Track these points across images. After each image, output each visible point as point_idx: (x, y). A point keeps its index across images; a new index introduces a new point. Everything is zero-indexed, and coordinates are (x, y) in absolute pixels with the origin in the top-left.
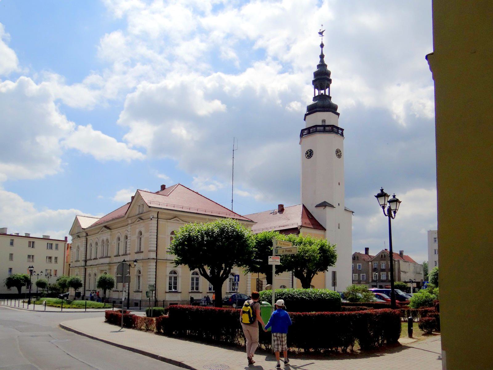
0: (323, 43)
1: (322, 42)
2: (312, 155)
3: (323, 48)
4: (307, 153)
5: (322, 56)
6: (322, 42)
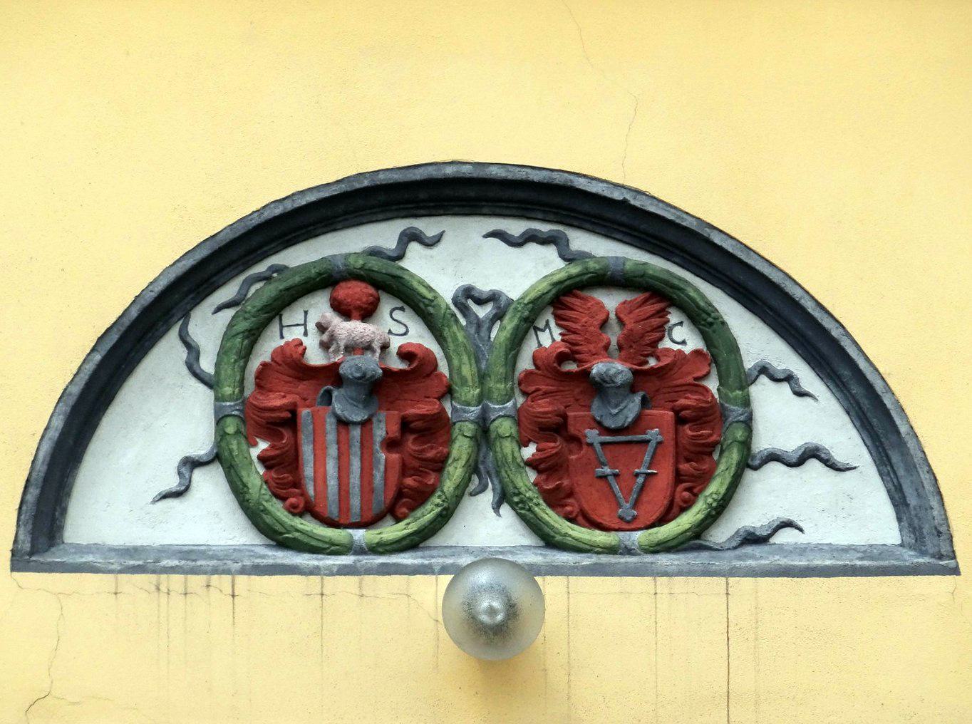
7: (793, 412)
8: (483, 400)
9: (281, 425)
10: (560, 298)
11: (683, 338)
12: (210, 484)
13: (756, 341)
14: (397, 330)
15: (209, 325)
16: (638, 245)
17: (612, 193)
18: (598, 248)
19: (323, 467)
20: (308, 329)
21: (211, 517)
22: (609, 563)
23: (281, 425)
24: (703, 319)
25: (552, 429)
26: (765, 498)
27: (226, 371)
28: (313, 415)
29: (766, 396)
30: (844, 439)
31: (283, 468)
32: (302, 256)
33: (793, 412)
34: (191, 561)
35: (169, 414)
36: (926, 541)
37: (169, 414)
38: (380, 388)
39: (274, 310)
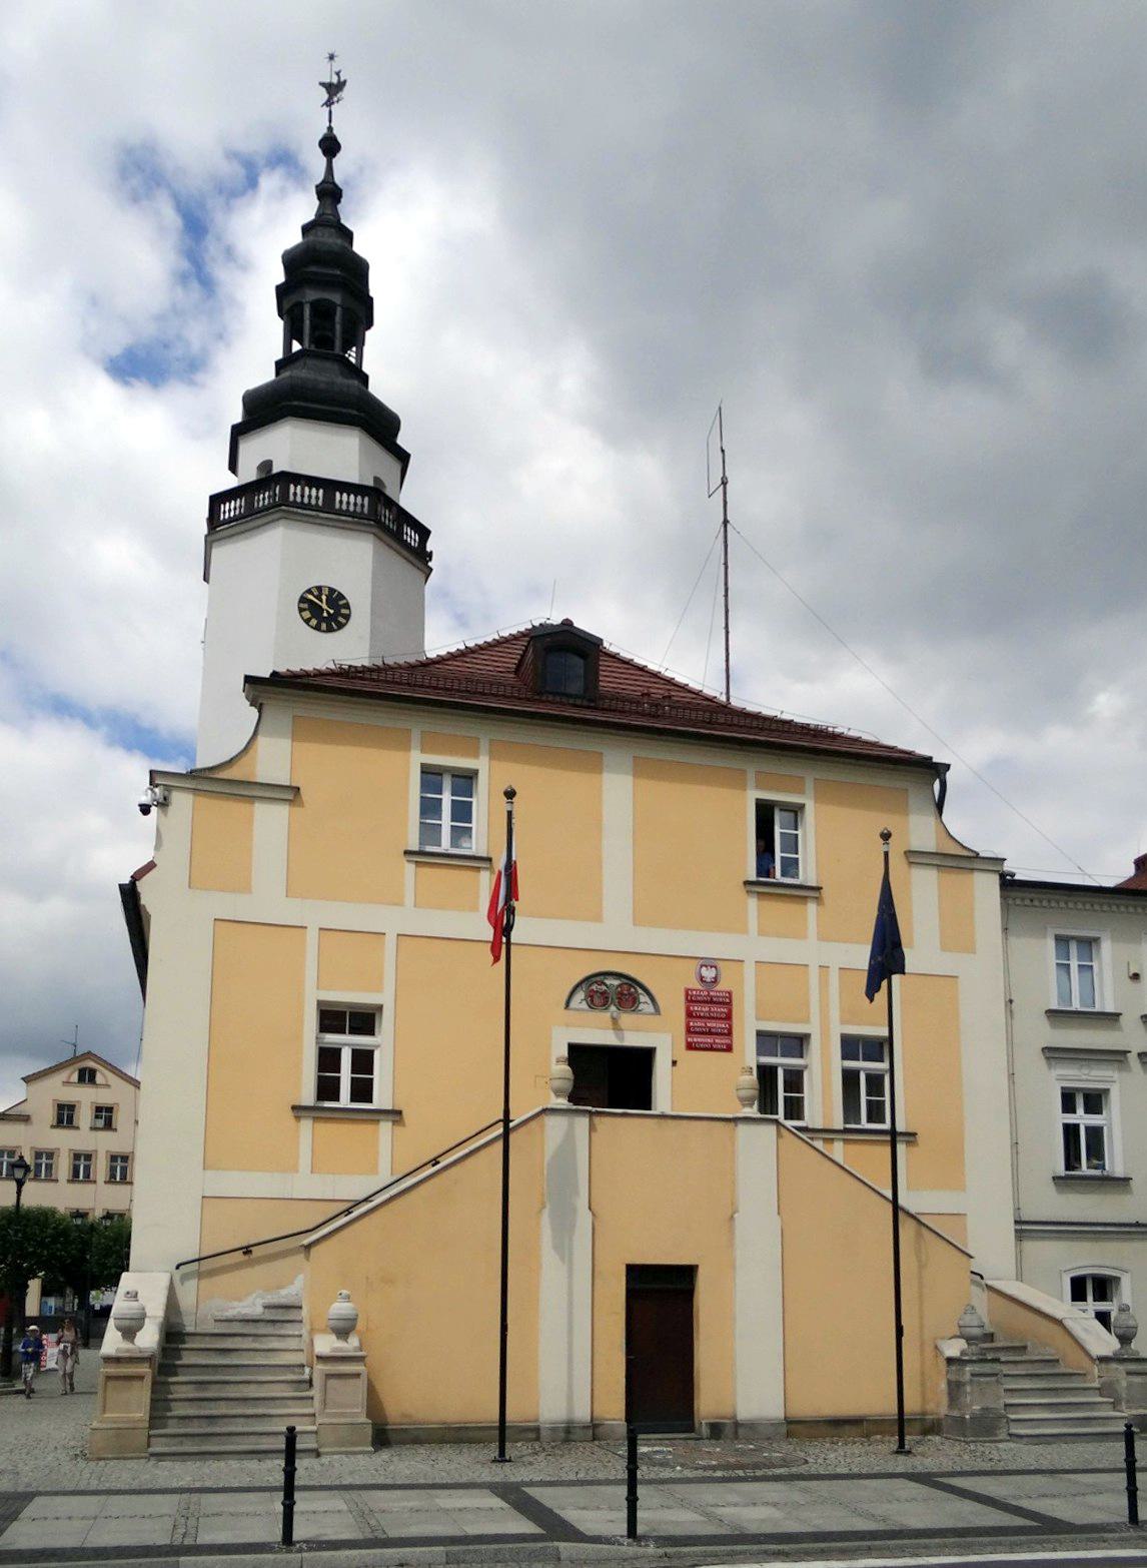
0: (335, 132)
1: (330, 129)
2: (307, 615)
3: (334, 161)
4: (336, 599)
5: (329, 193)
6: (330, 129)
7: (644, 998)
8: (613, 995)
9: (592, 997)
10: (620, 986)
11: (632, 990)
12: (584, 1002)
13: (640, 991)
14: (604, 988)
15: (584, 985)
16: (454, 665)
17: (1141, 1470)
18: (626, 981)
19: (597, 1000)
20: (594, 987)
21: (584, 1005)
22: (625, 1012)
23: (592, 997)
24: (635, 989)
25: (619, 998)
26: (641, 1007)
27: (58, 1250)
28: (141, 1378)
29: (641, 996)
30: (649, 1001)
31: (592, 1001)
32: (594, 979)
33: (644, 998)
34: (583, 1010)
35: (580, 995)
36: (657, 1011)
37: (580, 995)
38: (601, 993)
39: (591, 985)
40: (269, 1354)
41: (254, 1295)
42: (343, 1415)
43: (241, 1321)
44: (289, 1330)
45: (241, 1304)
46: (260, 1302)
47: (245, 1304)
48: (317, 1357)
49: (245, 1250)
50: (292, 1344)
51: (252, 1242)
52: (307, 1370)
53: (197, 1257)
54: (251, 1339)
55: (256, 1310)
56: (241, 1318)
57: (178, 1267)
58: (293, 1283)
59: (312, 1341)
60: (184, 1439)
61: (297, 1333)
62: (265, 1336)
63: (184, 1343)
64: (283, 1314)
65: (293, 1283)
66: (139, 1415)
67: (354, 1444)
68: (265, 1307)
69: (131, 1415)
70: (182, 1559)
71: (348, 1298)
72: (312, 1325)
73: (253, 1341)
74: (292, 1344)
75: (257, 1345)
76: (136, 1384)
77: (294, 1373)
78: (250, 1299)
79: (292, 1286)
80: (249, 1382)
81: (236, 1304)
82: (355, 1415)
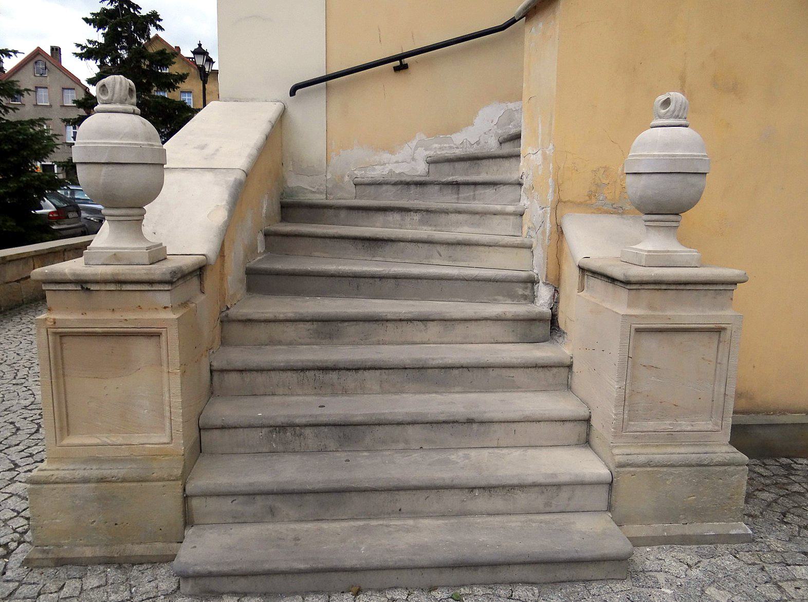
40: (459, 252)
41: (414, 143)
42: (672, 437)
43: (395, 184)
44: (487, 200)
45: (394, 158)
46: (422, 154)
47: (399, 157)
48: (582, 270)
49: (397, 63)
50: (499, 230)
51: (407, 49)
52: (544, 294)
53: (323, 74)
54: (417, 217)
55: (419, 169)
56: (395, 179)
57: (293, 92)
58: (473, 125)
59: (560, 231)
60: (278, 503)
61: (510, 208)
62: (446, 212)
63: (41, 208)
64: (467, 175)
65: (473, 125)
66: (158, 439)
67: (699, 514)
68: (429, 163)
69: (137, 439)
70: (405, 59)
71: (681, 119)
72: (558, 187)
73: (423, 222)
74: (499, 230)
75: (424, 232)
76: (143, 350)
77: (512, 296)
78: (405, 152)
79: (470, 128)
80: (425, 320)
81: (386, 156)
82: (701, 439)
